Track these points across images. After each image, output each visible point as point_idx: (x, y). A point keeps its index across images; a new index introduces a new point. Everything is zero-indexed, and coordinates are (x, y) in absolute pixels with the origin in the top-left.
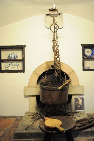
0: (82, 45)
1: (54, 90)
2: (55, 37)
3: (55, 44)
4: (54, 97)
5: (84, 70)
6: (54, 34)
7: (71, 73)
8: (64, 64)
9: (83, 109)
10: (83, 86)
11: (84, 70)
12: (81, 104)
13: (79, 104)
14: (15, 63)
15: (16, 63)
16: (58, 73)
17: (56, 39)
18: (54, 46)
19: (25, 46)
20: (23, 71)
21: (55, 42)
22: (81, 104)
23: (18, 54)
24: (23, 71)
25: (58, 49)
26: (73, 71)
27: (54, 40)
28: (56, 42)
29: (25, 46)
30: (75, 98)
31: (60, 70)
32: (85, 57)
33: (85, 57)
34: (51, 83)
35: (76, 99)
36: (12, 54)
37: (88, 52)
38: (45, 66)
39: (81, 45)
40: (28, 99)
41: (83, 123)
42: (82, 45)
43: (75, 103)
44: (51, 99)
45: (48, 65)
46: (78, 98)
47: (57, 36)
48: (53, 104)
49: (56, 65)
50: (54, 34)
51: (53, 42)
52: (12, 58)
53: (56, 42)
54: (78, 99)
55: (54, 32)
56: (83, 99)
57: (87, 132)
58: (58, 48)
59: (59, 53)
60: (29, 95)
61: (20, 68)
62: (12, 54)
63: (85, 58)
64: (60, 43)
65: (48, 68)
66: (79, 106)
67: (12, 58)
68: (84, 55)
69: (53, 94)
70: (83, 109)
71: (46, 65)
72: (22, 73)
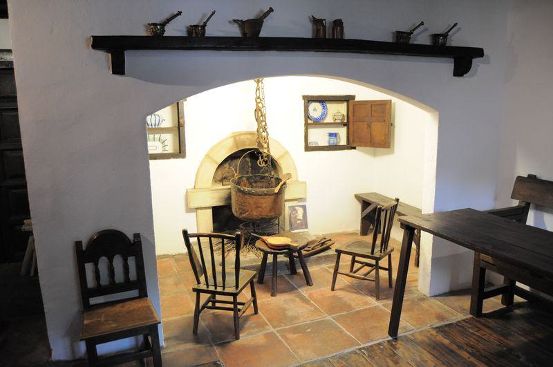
0: (304, 97)
1: (266, 195)
3: (260, 105)
4: (264, 206)
5: (308, 148)
7: (282, 157)
9: (306, 227)
10: (305, 183)
11: (308, 148)
14: (157, 136)
15: (153, 136)
16: (264, 161)
18: (258, 110)
20: (180, 152)
21: (259, 100)
26: (287, 152)
27: (259, 98)
31: (268, 156)
32: (309, 121)
33: (309, 121)
34: (247, 179)
35: (293, 208)
37: (315, 110)
38: (230, 143)
39: (302, 98)
40: (194, 214)
41: (312, 246)
42: (304, 97)
43: (290, 217)
44: (259, 209)
45: (235, 141)
46: (5, 150)
48: (262, 218)
49: (259, 143)
51: (256, 101)
52: (153, 123)
56: (304, 207)
57: (320, 257)
60: (199, 206)
63: (311, 123)
64: (267, 103)
65: (237, 147)
66: (299, 222)
67: (153, 123)
68: (307, 117)
69: (263, 201)
70: (306, 227)
71: (232, 140)
72: (180, 160)
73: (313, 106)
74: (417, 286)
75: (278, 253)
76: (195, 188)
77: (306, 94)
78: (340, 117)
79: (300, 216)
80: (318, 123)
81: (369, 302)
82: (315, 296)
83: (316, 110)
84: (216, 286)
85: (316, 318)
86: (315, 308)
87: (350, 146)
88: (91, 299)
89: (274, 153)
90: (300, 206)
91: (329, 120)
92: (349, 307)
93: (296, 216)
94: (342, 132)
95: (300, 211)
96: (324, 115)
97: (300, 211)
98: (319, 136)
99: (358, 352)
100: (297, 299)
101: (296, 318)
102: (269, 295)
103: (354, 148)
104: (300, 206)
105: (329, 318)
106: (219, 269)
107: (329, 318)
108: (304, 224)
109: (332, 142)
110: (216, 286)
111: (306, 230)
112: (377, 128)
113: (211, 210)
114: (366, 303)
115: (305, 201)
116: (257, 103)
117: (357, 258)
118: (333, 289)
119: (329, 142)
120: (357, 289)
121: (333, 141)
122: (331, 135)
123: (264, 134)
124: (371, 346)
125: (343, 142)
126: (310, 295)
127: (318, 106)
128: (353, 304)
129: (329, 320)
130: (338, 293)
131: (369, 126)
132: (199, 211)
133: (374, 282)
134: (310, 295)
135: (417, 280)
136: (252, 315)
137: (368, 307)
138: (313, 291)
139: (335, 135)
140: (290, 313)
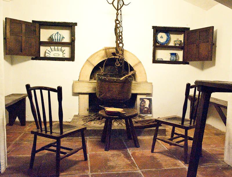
0: (154, 27)
1: (115, 82)
2: (119, 16)
3: (119, 25)
4: (114, 90)
5: (155, 61)
6: (118, 12)
7: (136, 65)
8: (127, 53)
9: (151, 113)
10: (151, 83)
11: (155, 61)
12: (148, 107)
13: (145, 106)
14: (60, 48)
16: (119, 63)
17: (119, 19)
18: (116, 28)
19: (76, 24)
20: (72, 58)
21: (118, 22)
22: (148, 107)
23: (65, 35)
24: (72, 58)
25: (122, 32)
26: (140, 62)
28: (119, 22)
29: (76, 24)
30: (141, 99)
32: (157, 44)
36: (57, 35)
37: (162, 37)
40: (77, 98)
42: (154, 27)
45: (106, 52)
47: (121, 14)
50: (118, 12)
53: (119, 22)
54: (145, 100)
55: (118, 10)
56: (150, 100)
58: (122, 31)
59: (122, 38)
61: (67, 55)
62: (57, 35)
63: (157, 46)
64: (124, 24)
66: (146, 109)
68: (155, 40)
71: (103, 52)
73: (160, 35)
74: (223, 158)
75: (113, 118)
76: (79, 81)
77: (155, 25)
78: (179, 43)
79: (147, 105)
80: (164, 46)
81: (178, 164)
82: (136, 154)
83: (162, 38)
84: (46, 131)
85: (129, 170)
86: (133, 163)
87: (185, 62)
88: (33, 90)
89: (131, 62)
90: (148, 99)
91: (172, 44)
92: (159, 165)
93: (144, 105)
94: (180, 54)
95: (147, 102)
96: (168, 40)
97: (147, 102)
98: (164, 54)
99: (8, 154)
100: (122, 155)
101: (113, 167)
102: (104, 150)
103: (188, 63)
104: (148, 99)
105: (140, 171)
106: (48, 119)
107: (140, 171)
108: (149, 111)
109: (172, 59)
110: (46, 131)
111: (151, 115)
112: (203, 48)
113: (88, 95)
114: (175, 165)
115: (152, 96)
116: (116, 24)
117: (66, 52)
118: (152, 151)
119: (170, 59)
120: (170, 154)
121: (173, 58)
122: (172, 54)
123: (121, 45)
124: (7, 137)
125: (181, 59)
126: (133, 154)
127: (164, 35)
128: (164, 164)
129: (139, 173)
130: (155, 155)
131: (198, 47)
132: (80, 95)
133: (183, 149)
134: (133, 154)
135: (223, 154)
136: (82, 161)
137: (176, 168)
138: (136, 151)
139: (175, 54)
140: (110, 164)
